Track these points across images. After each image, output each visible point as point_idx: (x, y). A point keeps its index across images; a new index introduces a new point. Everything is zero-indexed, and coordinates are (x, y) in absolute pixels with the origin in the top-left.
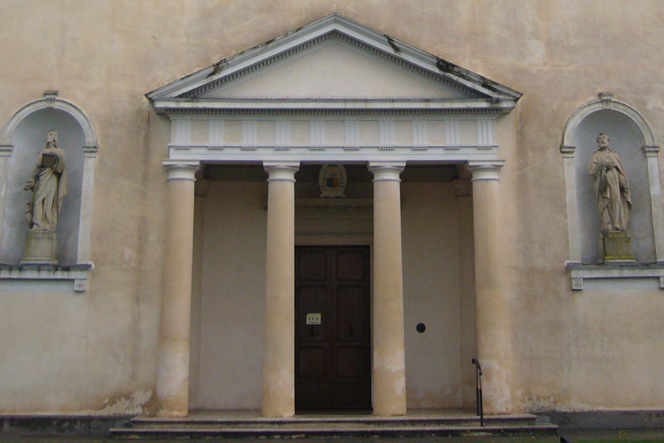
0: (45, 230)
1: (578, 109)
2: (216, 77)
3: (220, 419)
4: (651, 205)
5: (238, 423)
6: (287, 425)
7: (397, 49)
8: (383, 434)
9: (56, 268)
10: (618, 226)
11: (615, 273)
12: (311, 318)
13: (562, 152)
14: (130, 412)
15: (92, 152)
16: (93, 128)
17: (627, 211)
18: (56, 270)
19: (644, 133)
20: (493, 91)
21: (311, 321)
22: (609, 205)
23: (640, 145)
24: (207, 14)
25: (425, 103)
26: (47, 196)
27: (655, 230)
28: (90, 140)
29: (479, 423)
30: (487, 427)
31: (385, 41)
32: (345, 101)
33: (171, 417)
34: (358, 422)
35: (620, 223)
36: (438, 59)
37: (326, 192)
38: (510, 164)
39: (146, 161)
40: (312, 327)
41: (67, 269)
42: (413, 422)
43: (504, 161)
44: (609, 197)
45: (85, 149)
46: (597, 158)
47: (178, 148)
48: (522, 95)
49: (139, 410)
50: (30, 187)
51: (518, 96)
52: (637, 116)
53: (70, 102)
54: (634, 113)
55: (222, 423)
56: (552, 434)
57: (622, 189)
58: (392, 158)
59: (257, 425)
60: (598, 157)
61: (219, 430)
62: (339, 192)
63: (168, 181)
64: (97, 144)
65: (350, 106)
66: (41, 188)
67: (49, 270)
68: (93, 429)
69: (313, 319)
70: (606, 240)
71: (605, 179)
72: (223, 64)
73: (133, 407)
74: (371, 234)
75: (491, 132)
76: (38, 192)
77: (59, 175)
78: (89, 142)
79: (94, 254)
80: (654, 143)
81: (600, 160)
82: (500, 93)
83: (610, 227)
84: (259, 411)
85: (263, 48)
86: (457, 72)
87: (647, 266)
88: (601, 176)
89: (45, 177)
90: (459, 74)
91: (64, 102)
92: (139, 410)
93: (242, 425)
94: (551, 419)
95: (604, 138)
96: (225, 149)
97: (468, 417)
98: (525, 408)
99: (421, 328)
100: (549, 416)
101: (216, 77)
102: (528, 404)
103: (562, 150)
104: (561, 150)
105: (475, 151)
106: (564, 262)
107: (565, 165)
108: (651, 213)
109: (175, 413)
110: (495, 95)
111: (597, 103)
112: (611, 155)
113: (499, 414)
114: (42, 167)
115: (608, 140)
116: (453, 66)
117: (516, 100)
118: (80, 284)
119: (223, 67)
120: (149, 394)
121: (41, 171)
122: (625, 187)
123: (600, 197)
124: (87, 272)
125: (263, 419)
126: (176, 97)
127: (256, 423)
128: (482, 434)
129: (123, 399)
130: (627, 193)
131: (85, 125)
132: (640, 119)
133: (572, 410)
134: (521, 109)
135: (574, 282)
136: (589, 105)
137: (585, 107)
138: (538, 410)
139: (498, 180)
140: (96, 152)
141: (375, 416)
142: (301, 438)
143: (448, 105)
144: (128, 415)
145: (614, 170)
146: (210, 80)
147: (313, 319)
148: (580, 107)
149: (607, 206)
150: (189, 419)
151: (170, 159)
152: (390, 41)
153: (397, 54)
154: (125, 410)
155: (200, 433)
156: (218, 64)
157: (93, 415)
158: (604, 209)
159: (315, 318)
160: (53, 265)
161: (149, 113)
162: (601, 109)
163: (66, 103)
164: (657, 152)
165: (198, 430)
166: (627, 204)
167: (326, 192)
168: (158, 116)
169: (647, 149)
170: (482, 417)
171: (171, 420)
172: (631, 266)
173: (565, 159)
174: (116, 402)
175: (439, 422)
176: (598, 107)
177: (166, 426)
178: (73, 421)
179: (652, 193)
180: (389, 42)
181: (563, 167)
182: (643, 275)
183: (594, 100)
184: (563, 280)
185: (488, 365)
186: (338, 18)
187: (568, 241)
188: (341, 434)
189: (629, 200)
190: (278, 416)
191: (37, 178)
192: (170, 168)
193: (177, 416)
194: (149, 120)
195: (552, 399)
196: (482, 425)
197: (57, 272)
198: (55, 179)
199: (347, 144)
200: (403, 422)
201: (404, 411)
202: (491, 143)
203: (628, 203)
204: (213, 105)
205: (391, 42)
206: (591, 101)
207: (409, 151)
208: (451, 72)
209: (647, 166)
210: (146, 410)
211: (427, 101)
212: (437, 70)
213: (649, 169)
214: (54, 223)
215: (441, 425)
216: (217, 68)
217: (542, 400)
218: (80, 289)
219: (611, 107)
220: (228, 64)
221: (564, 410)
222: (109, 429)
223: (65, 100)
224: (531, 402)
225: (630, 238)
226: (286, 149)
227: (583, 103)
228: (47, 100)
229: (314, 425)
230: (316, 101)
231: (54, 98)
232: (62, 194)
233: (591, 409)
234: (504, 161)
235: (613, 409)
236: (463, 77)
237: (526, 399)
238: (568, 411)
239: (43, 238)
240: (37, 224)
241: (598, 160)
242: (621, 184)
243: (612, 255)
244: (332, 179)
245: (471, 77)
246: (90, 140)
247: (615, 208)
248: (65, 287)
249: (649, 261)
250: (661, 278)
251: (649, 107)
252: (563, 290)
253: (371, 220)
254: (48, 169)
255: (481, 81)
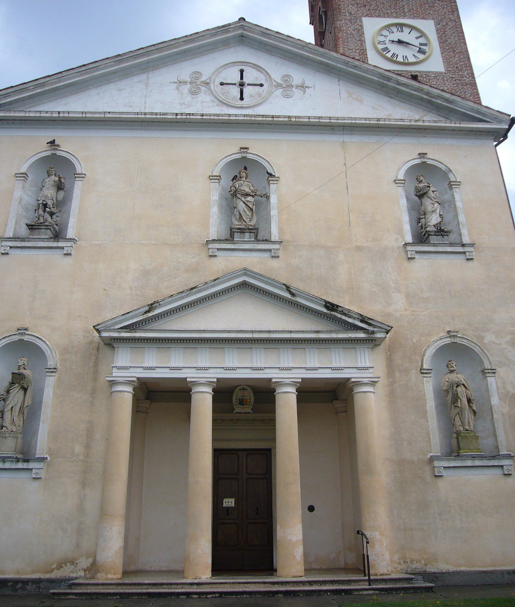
0: (12, 431)
1: (433, 342)
2: (150, 314)
3: (146, 582)
4: (492, 412)
5: (162, 584)
6: (205, 586)
7: (293, 295)
8: (286, 593)
9: (18, 460)
10: (467, 427)
11: (469, 463)
12: (227, 502)
13: (422, 373)
14: (74, 575)
15: (53, 372)
16: (54, 354)
17: (473, 417)
18: (18, 461)
19: (483, 359)
20: (369, 325)
21: (227, 504)
22: (460, 412)
23: (480, 369)
24: (146, 273)
25: (316, 334)
26: (15, 405)
27: (496, 430)
28: (51, 363)
29: (367, 583)
30: (374, 586)
31: (284, 289)
32: (253, 332)
33: (107, 579)
34: (265, 583)
35: (469, 426)
36: (325, 301)
37: (238, 409)
38: (383, 382)
39: (95, 379)
40: (228, 508)
41: (27, 461)
42: (310, 583)
43: (379, 378)
44: (460, 406)
45: (47, 370)
46: (448, 378)
47: (119, 368)
48: (392, 327)
49: (82, 573)
50: (3, 398)
51: (389, 328)
52: (477, 347)
53: (37, 335)
54: (475, 345)
55: (149, 584)
56: (429, 592)
57: (469, 401)
58: (290, 376)
59: (179, 586)
60: (449, 378)
61: (145, 591)
62: (248, 409)
63: (111, 393)
64: (57, 367)
65: (256, 336)
66: (10, 399)
67: (11, 461)
68: (42, 589)
69: (228, 502)
70: (460, 438)
71: (456, 392)
72: (156, 304)
73: (76, 571)
74: (274, 440)
75: (367, 355)
76: (8, 402)
77: (25, 390)
78: (50, 365)
79: (50, 449)
80: (492, 366)
81: (450, 379)
82: (374, 326)
83: (462, 429)
84: (181, 573)
85: (188, 293)
86: (340, 311)
87: (493, 457)
88: (453, 390)
89: (14, 391)
90: (342, 313)
91: (32, 335)
92: (82, 573)
93: (166, 587)
94: (423, 578)
95: (453, 364)
96: (210, 369)
97: (358, 578)
98: (402, 570)
99: (311, 509)
100: (421, 575)
101: (150, 314)
102: (404, 566)
103: (422, 371)
104: (421, 371)
105: (355, 370)
106: (428, 455)
107: (425, 382)
108: (492, 418)
109: (110, 576)
110: (371, 329)
111: (446, 337)
112: (458, 375)
113: (382, 575)
114: (12, 383)
115: (456, 365)
116: (338, 306)
117: (387, 332)
118: (37, 472)
119: (156, 307)
120: (90, 560)
121: (11, 386)
122: (472, 398)
123: (453, 407)
124: (43, 463)
125: (184, 581)
126: (118, 329)
127: (177, 584)
128: (371, 592)
129: (68, 564)
130: (473, 403)
131: (48, 353)
132: (479, 350)
133: (439, 571)
134: (389, 342)
135: (436, 469)
136: (441, 339)
137: (438, 340)
138: (412, 571)
139: (374, 393)
140: (56, 372)
141: (278, 577)
142: (216, 597)
143: (334, 336)
144: (72, 577)
145: (462, 386)
146: (145, 316)
147: (228, 502)
148: (434, 341)
149: (458, 413)
150: (120, 581)
151: (113, 375)
152: (288, 289)
153: (293, 298)
154: (70, 573)
155: (128, 594)
156: (152, 304)
157: (43, 577)
158: (456, 415)
159: (230, 502)
160: (16, 457)
161: (99, 344)
162: (450, 342)
163: (34, 336)
164: (494, 373)
165: (127, 591)
166: (472, 412)
167: (238, 409)
168: (105, 345)
169: (487, 371)
170: (369, 577)
171: (105, 582)
172: (482, 457)
173: (424, 378)
174: (62, 567)
175: (332, 582)
176: (448, 341)
177: (100, 587)
178: (25, 582)
179: (492, 403)
180: (287, 289)
181: (423, 384)
182: (490, 465)
183: (444, 336)
184: (428, 468)
185: (371, 535)
186: (247, 272)
187: (430, 439)
188: (250, 593)
189: (474, 408)
190: (197, 578)
191: (8, 392)
192: (113, 383)
193: (111, 579)
194: (98, 349)
195: (423, 561)
196: (370, 585)
197: (19, 463)
198: (22, 392)
199: (255, 365)
200: (303, 583)
201: (302, 573)
202: (368, 365)
203: (474, 411)
204: (147, 335)
205: (289, 289)
206: (442, 336)
207: (303, 371)
208: (336, 311)
209: (487, 384)
210: (87, 573)
211: (318, 332)
212: (325, 310)
213: (489, 386)
214: (20, 426)
215: (334, 585)
216: (151, 307)
217: (415, 563)
218: (37, 477)
219: (457, 340)
220: (160, 304)
221: (433, 570)
222: (50, 590)
223: (33, 334)
224: (406, 565)
225: (478, 436)
226: (206, 369)
227: (436, 337)
228: (19, 333)
229: (226, 585)
230: (229, 332)
231: (25, 332)
232: (27, 403)
233: (455, 570)
234: (379, 378)
235: (473, 569)
236: (345, 315)
237: (402, 562)
238: (437, 571)
239: (10, 437)
240: (5, 427)
241: (449, 380)
242: (468, 397)
243: (465, 450)
244: (243, 399)
245: (352, 315)
246: (51, 363)
247: (465, 414)
248: (24, 475)
249: (495, 454)
250: (504, 466)
251: (486, 341)
252: (428, 477)
253: (274, 430)
254: (17, 385)
255: (360, 318)
